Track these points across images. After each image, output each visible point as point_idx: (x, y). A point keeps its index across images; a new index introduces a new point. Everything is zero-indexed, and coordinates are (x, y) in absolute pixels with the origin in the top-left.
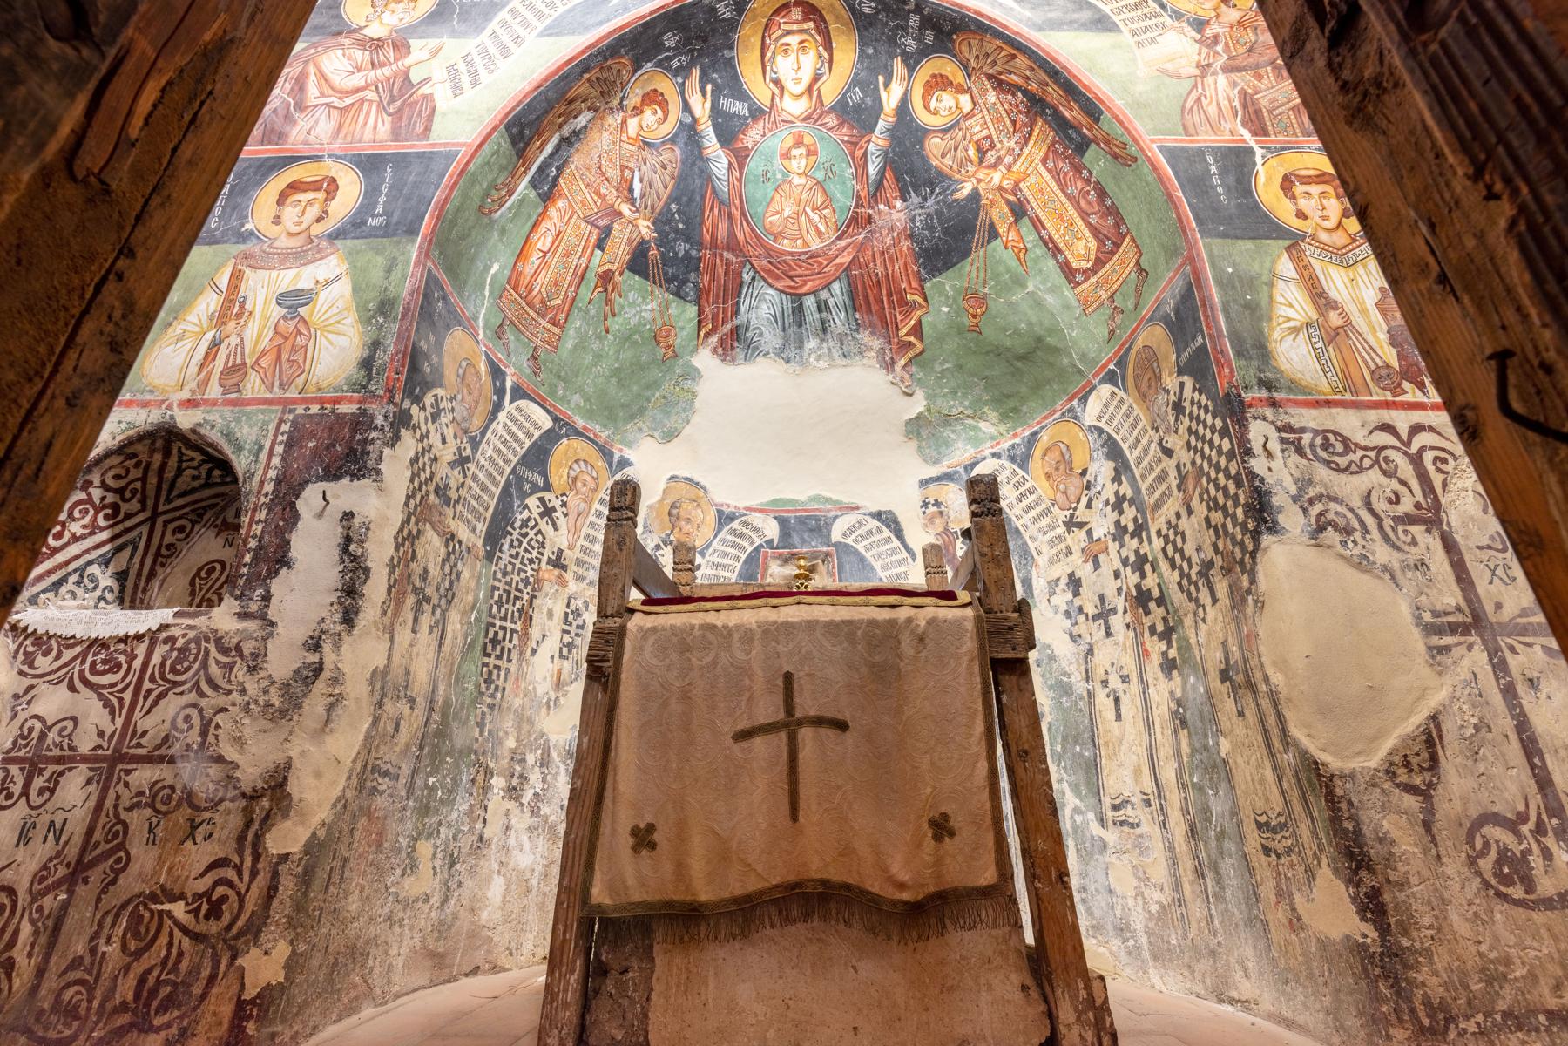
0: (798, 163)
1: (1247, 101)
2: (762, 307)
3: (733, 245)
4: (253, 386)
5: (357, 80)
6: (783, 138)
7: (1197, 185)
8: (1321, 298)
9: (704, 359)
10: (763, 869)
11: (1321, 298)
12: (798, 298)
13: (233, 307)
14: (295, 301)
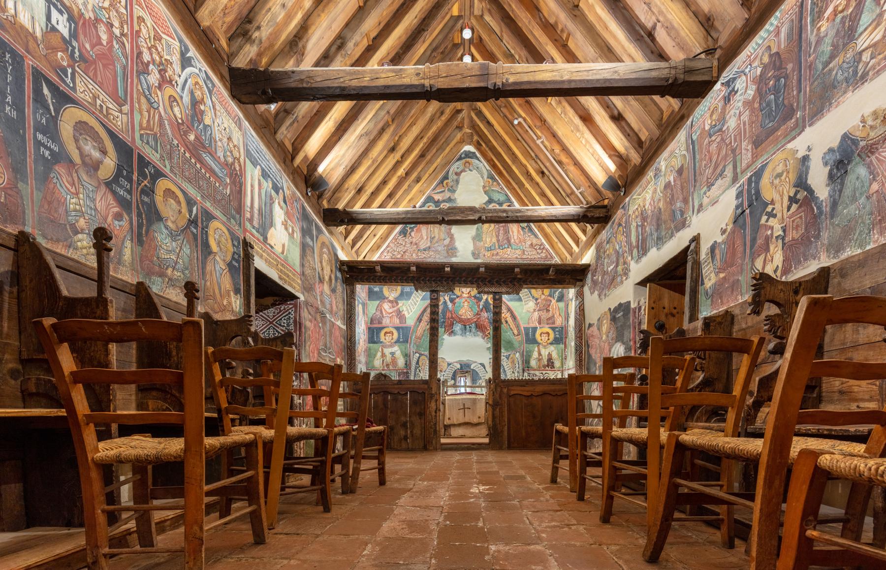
0: (466, 304)
1: (540, 318)
2: (458, 327)
3: (452, 318)
4: (391, 367)
5: (391, 311)
6: (463, 300)
7: (527, 334)
8: (540, 354)
9: (446, 337)
10: (461, 421)
11: (540, 354)
12: (465, 326)
13: (383, 355)
14: (393, 354)
